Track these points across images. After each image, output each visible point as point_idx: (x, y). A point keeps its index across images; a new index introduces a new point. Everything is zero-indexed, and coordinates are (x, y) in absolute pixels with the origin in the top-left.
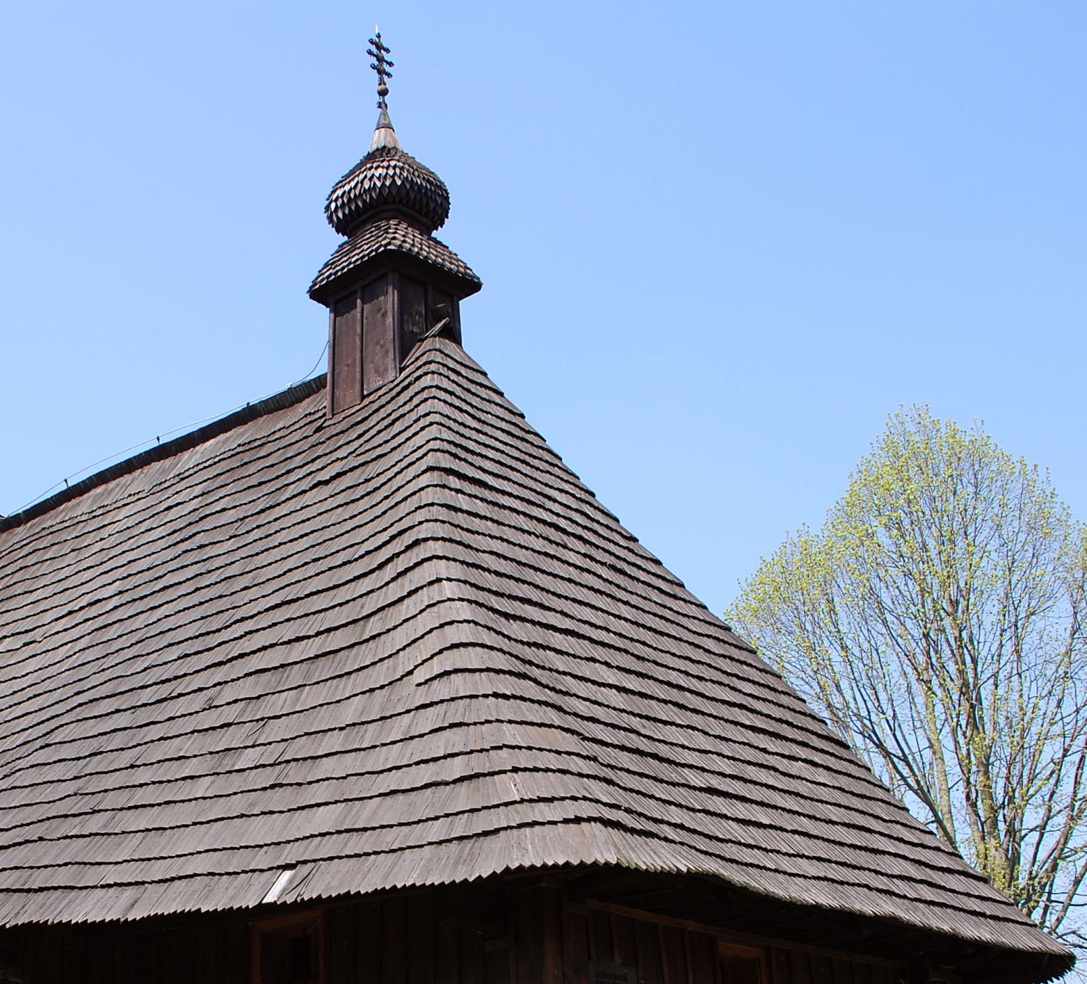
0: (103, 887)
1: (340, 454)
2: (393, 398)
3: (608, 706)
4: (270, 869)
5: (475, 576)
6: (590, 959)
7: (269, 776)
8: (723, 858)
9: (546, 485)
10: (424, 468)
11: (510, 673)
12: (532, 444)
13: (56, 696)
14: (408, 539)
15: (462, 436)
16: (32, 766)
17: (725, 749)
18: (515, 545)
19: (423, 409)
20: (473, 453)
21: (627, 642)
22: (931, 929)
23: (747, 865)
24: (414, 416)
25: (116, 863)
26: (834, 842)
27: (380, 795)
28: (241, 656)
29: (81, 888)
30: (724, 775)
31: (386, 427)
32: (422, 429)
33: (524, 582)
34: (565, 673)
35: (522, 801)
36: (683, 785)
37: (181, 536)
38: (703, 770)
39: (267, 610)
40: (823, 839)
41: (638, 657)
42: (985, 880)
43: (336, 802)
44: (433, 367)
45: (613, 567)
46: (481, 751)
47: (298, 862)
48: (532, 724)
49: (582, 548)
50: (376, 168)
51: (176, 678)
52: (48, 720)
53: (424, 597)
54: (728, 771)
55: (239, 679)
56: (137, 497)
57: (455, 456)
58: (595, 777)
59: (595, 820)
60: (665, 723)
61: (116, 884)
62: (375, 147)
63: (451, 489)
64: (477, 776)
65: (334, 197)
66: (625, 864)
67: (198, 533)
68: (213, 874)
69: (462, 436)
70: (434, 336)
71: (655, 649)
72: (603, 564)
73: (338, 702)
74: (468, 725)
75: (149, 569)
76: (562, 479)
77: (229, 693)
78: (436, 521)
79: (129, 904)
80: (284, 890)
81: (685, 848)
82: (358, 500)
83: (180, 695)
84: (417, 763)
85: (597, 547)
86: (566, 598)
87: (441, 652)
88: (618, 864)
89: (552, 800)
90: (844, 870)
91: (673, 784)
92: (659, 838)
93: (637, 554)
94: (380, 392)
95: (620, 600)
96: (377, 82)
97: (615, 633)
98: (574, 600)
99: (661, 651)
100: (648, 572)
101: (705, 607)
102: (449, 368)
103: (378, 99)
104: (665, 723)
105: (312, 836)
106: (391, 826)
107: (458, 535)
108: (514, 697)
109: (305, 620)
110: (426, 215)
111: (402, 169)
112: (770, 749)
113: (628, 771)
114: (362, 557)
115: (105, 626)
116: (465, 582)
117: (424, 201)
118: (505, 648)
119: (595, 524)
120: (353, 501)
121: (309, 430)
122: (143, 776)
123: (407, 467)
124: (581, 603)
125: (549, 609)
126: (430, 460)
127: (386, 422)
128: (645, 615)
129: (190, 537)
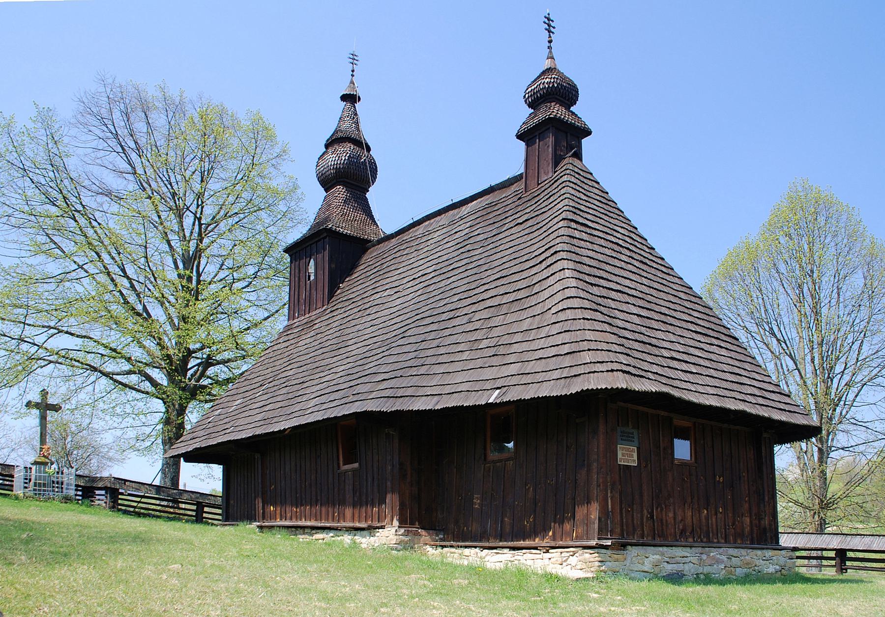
0: (425, 396)
1: (528, 210)
2: (551, 186)
3: (632, 323)
4: (491, 389)
5: (579, 267)
6: (619, 426)
7: (492, 352)
8: (673, 386)
9: (615, 225)
10: (561, 219)
11: (591, 309)
12: (611, 206)
13: (408, 316)
14: (552, 251)
15: (579, 203)
16: (398, 346)
17: (682, 341)
18: (598, 253)
19: (562, 191)
20: (583, 211)
21: (644, 295)
22: (759, 416)
23: (683, 389)
24: (559, 194)
25: (431, 386)
26: (724, 380)
27: (535, 360)
28: (483, 300)
29: (417, 396)
30: (679, 352)
31: (547, 199)
32: (562, 201)
33: (601, 269)
34: (615, 309)
35: (591, 363)
36: (661, 356)
37: (461, 245)
38: (670, 349)
39: (494, 280)
40: (719, 379)
41: (648, 301)
42: (789, 396)
43: (518, 362)
44: (568, 172)
45: (641, 262)
46: (576, 342)
47: (502, 386)
48: (598, 331)
49: (628, 253)
50: (546, 79)
51: (456, 309)
52: (405, 326)
53: (557, 277)
54: (681, 350)
55: (481, 310)
56: (443, 227)
57: (575, 213)
58: (622, 353)
59: (619, 370)
60: (657, 330)
61: (431, 395)
62: (546, 68)
63: (572, 228)
64: (574, 352)
65: (527, 92)
66: (629, 388)
67: (468, 244)
68: (469, 391)
69: (579, 203)
70: (570, 157)
71: (656, 298)
72: (637, 260)
73: (521, 320)
74: (572, 331)
75: (447, 260)
76: (623, 222)
77: (477, 316)
78: (564, 243)
79: (435, 403)
80: (496, 397)
81: (657, 382)
82: (533, 232)
83: (458, 316)
84: (550, 347)
85: (636, 253)
86: (619, 276)
87: (563, 300)
88: (626, 388)
89: (603, 362)
90: (726, 391)
91: (656, 356)
92: (646, 378)
93: (654, 256)
94: (546, 182)
95: (643, 276)
96: (548, 36)
97: (639, 291)
98: (622, 277)
99: (659, 298)
100: (658, 264)
101: (682, 279)
102: (575, 172)
103: (548, 44)
104: (657, 330)
105: (508, 376)
106: (539, 372)
107: (573, 249)
108: (591, 319)
109: (510, 285)
110: (568, 100)
111: (557, 79)
112: (702, 341)
113: (637, 350)
114: (533, 258)
115: (428, 285)
116: (575, 270)
117: (567, 94)
118: (589, 299)
119: (636, 242)
120: (531, 233)
121: (515, 199)
122: (442, 350)
123: (554, 218)
124: (625, 278)
125: (611, 281)
126: (564, 215)
127: (547, 197)
128: (654, 283)
129: (464, 246)
